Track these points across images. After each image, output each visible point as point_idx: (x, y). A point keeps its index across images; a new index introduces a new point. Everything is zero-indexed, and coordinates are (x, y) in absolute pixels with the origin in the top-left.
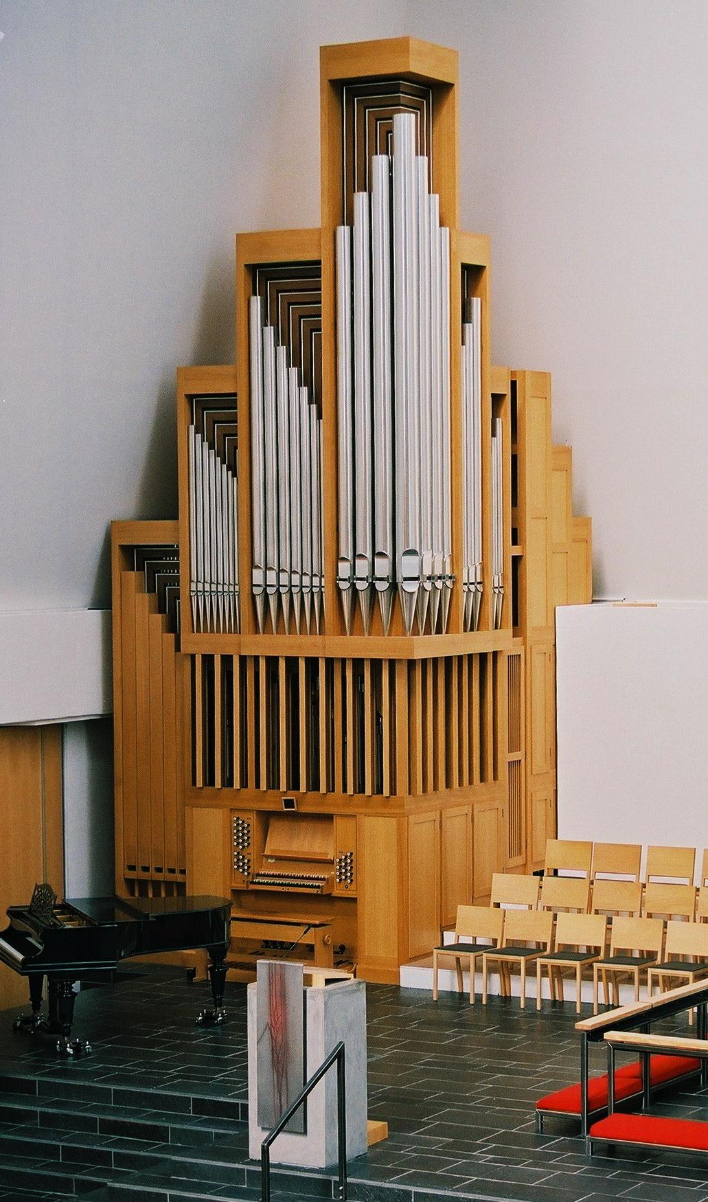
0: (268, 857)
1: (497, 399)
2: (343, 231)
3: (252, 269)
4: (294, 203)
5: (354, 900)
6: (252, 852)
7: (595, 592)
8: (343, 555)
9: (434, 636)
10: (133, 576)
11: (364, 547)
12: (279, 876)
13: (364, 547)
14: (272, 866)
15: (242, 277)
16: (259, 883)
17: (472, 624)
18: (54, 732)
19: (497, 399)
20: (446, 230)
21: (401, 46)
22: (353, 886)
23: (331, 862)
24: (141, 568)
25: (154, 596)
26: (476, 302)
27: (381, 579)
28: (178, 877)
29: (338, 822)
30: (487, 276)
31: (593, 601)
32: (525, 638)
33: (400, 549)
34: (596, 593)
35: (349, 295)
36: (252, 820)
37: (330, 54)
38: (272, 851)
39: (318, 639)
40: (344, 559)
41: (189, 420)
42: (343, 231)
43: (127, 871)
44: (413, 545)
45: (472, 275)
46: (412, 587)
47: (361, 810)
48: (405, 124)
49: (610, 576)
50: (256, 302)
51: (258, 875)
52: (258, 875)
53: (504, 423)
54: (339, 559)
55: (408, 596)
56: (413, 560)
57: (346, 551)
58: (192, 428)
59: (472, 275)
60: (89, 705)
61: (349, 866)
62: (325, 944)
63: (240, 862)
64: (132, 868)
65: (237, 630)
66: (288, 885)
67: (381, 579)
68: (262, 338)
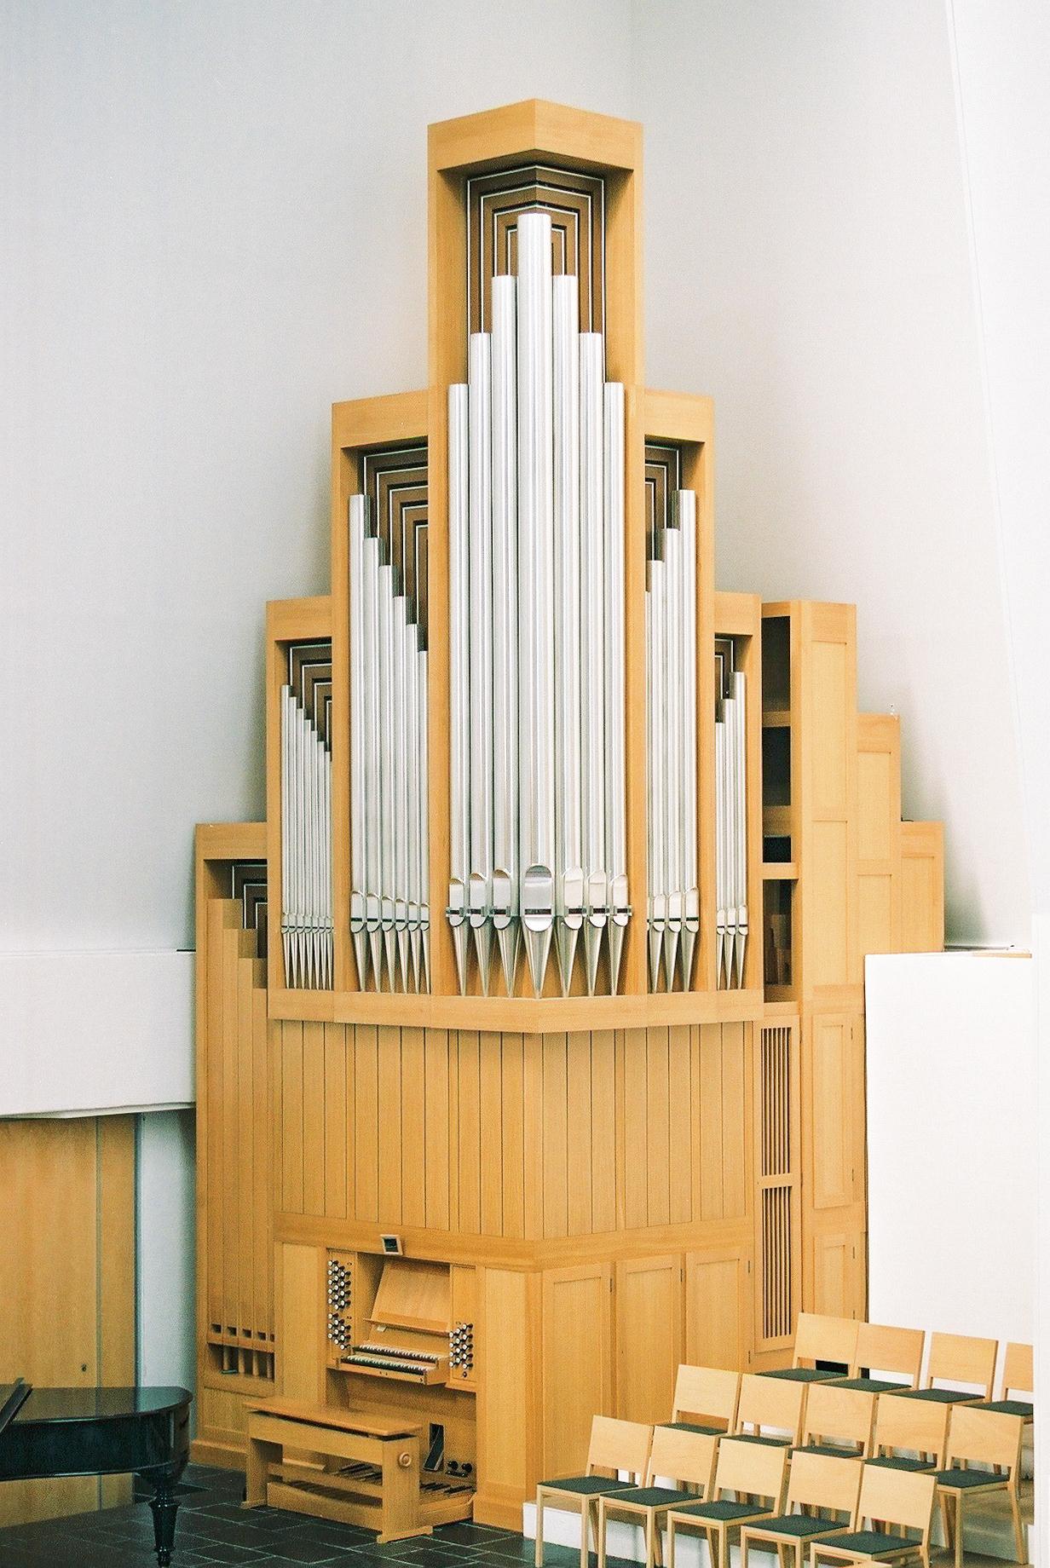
0: (377, 1324)
1: (730, 647)
2: (458, 390)
3: (357, 454)
4: (377, 353)
5: (472, 1395)
6: (353, 1315)
7: (949, 934)
8: (455, 874)
9: (670, 994)
10: (221, 904)
11: (482, 865)
12: (383, 1353)
13: (482, 865)
14: (378, 1339)
15: (341, 468)
16: (353, 1362)
17: (680, 975)
18: (130, 1123)
19: (730, 647)
20: (616, 390)
21: (524, 113)
22: (471, 1374)
23: (446, 1336)
24: (239, 895)
25: (253, 933)
26: (687, 497)
27: (477, 912)
28: (266, 1346)
29: (456, 1275)
30: (706, 454)
31: (947, 948)
32: (801, 1003)
33: (526, 864)
34: (957, 932)
35: (465, 485)
36: (353, 1265)
37: (442, 134)
38: (381, 1314)
39: (418, 1000)
40: (457, 881)
41: (284, 678)
42: (458, 390)
43: (212, 1333)
44: (545, 858)
45: (673, 459)
46: (542, 924)
47: (482, 1259)
48: (535, 228)
49: (993, 906)
50: (358, 503)
51: (357, 1349)
52: (357, 1349)
53: (749, 679)
54: (451, 880)
55: (536, 937)
56: (546, 883)
57: (459, 869)
58: (286, 689)
59: (673, 459)
60: (173, 1091)
61: (466, 1343)
62: (401, 1466)
63: (341, 1331)
64: (218, 1328)
65: (330, 986)
66: (388, 1367)
67: (477, 912)
68: (365, 551)
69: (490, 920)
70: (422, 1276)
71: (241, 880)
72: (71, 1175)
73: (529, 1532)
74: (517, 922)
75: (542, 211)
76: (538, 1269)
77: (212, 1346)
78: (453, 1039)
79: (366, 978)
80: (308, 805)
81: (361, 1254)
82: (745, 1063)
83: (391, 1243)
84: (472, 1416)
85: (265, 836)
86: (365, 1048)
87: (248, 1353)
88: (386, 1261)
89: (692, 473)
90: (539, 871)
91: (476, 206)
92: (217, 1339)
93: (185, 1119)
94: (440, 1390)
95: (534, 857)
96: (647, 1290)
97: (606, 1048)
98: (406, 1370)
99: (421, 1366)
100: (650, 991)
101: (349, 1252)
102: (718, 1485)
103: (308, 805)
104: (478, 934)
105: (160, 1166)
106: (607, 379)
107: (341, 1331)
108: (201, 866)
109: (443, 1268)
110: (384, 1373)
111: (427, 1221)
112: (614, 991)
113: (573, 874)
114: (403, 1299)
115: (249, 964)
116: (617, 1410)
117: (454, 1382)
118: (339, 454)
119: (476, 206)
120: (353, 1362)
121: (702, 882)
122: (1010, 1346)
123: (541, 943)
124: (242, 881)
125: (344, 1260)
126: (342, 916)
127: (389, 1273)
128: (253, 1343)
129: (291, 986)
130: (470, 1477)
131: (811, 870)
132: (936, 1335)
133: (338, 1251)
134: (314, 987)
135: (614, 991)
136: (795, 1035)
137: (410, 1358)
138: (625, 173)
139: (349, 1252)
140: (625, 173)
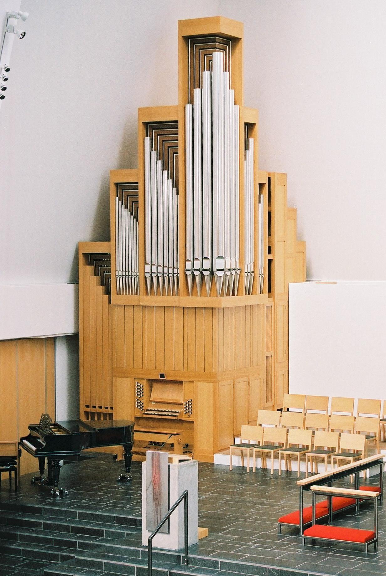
0: (152, 401)
3: (146, 124)
5: (193, 422)
6: (145, 399)
11: (198, 255)
12: (157, 411)
13: (198, 255)
16: (147, 414)
18: (53, 340)
21: (216, 20)
22: (192, 416)
23: (182, 404)
25: (99, 277)
28: (109, 411)
34: (308, 278)
35: (190, 137)
36: (145, 384)
37: (182, 24)
42: (189, 107)
46: (220, 274)
47: (196, 379)
48: (218, 57)
49: (315, 269)
50: (148, 140)
51: (147, 410)
52: (147, 410)
58: (117, 198)
60: (69, 329)
61: (190, 406)
62: (179, 443)
64: (88, 406)
65: (137, 293)
68: (151, 157)
70: (169, 386)
71: (99, 262)
72: (32, 359)
73: (216, 462)
74: (212, 273)
76: (216, 382)
78: (185, 310)
79: (190, 290)
81: (147, 379)
82: (261, 315)
83: (162, 376)
84: (193, 429)
85: (110, 246)
86: (150, 315)
88: (162, 380)
92: (87, 410)
93: (73, 341)
95: (218, 252)
96: (241, 387)
97: (226, 312)
100: (246, 294)
101: (143, 379)
102: (288, 443)
104: (165, 278)
105: (62, 354)
108: (81, 258)
109: (181, 383)
110: (160, 417)
111: (174, 367)
113: (228, 259)
114: (161, 393)
115: (101, 288)
116: (249, 423)
117: (185, 418)
118: (141, 124)
120: (147, 414)
121: (253, 262)
122: (333, 398)
123: (220, 279)
124: (93, 260)
125: (141, 382)
126: (142, 272)
127: (156, 386)
128: (103, 410)
129: (120, 294)
130: (188, 448)
133: (139, 379)
135: (231, 294)
136: (273, 307)
139: (143, 379)
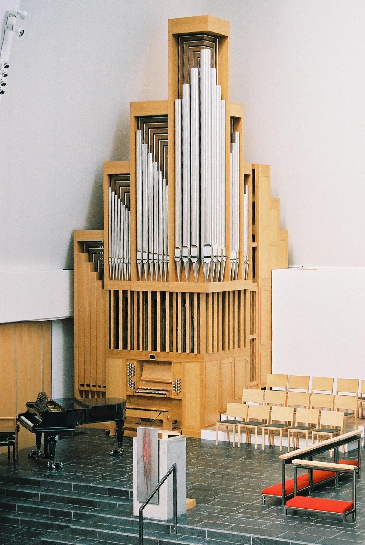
0: (143, 381)
1: (246, 177)
3: (137, 118)
4: (155, 88)
5: (181, 400)
6: (136, 378)
7: (289, 263)
11: (186, 243)
13: (186, 243)
16: (139, 392)
18: (50, 323)
19: (246, 177)
20: (224, 101)
21: (204, 19)
23: (171, 383)
28: (102, 389)
29: (174, 365)
33: (203, 244)
34: (290, 264)
36: (136, 364)
37: (172, 23)
38: (145, 378)
39: (166, 283)
45: (235, 121)
46: (208, 261)
47: (185, 360)
48: (206, 54)
50: (139, 133)
51: (138, 389)
52: (138, 389)
55: (206, 264)
58: (110, 189)
59: (235, 121)
61: (178, 385)
62: (168, 419)
63: (131, 384)
64: (82, 385)
68: (142, 149)
69: (190, 260)
75: (206, 48)
77: (80, 391)
80: (119, 224)
84: (181, 406)
85: (103, 234)
87: (93, 393)
89: (238, 126)
90: (208, 245)
91: (182, 44)
92: (82, 388)
94: (170, 399)
98: (156, 394)
99: (164, 393)
100: (231, 280)
103: (119, 224)
105: (58, 337)
106: (222, 99)
107: (131, 384)
110: (151, 395)
112: (212, 281)
113: (215, 247)
115: (95, 274)
116: (234, 401)
117: (174, 396)
119: (182, 44)
128: (97, 389)
131: (262, 244)
132: (313, 378)
134: (121, 280)
137: (158, 390)
138: (227, 37)
140: (227, 37)
